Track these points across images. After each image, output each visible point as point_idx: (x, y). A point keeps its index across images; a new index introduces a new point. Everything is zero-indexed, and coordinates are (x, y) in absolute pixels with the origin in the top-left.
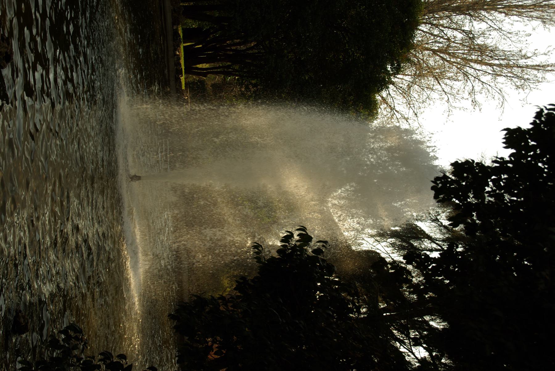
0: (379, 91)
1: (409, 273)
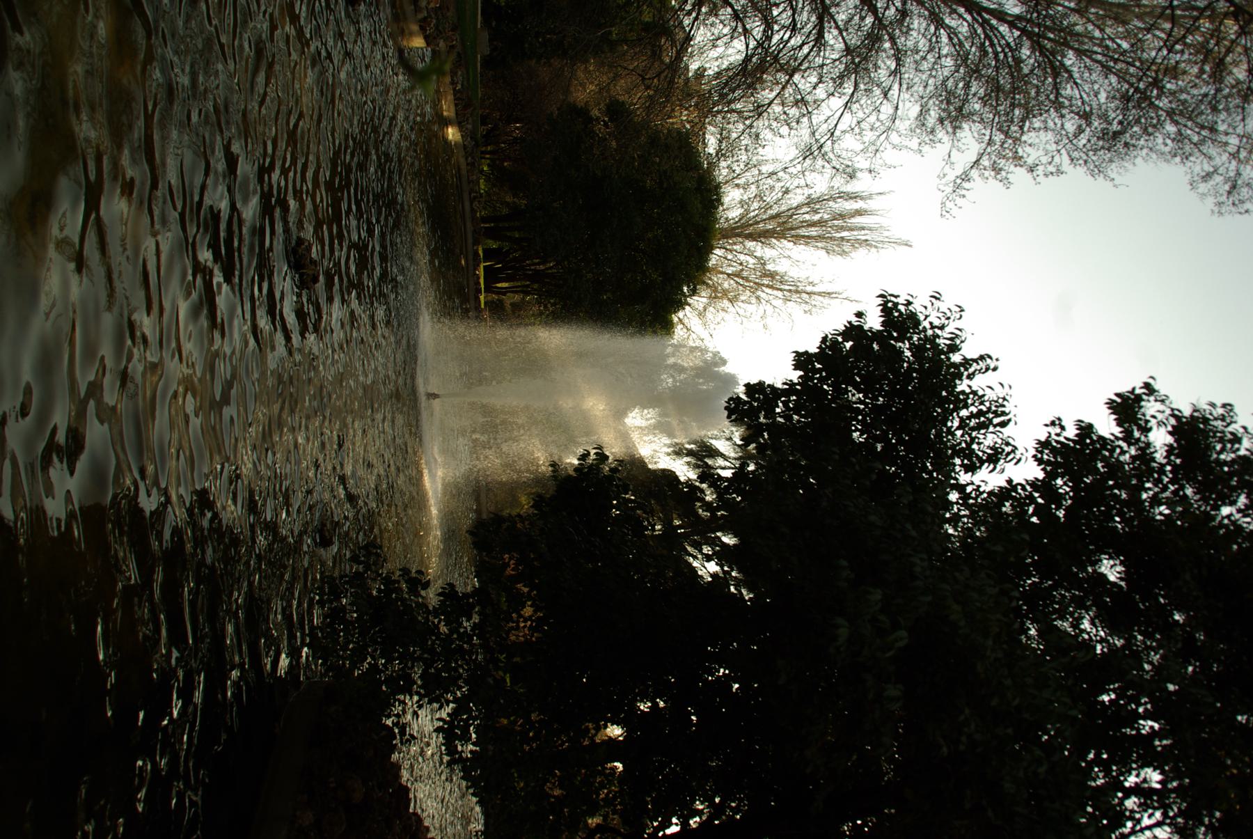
0: (675, 312)
1: (702, 491)
